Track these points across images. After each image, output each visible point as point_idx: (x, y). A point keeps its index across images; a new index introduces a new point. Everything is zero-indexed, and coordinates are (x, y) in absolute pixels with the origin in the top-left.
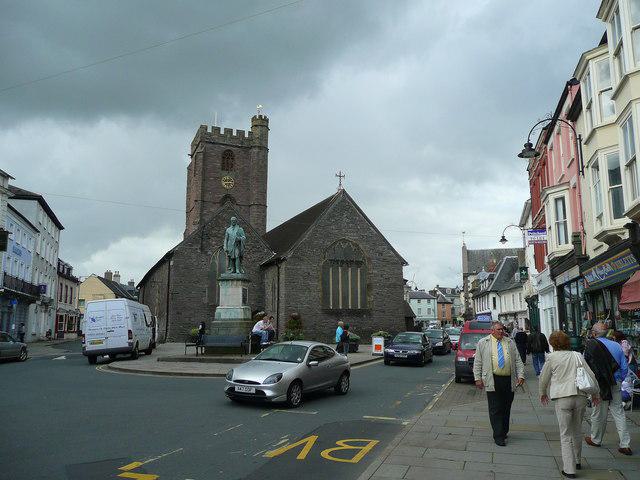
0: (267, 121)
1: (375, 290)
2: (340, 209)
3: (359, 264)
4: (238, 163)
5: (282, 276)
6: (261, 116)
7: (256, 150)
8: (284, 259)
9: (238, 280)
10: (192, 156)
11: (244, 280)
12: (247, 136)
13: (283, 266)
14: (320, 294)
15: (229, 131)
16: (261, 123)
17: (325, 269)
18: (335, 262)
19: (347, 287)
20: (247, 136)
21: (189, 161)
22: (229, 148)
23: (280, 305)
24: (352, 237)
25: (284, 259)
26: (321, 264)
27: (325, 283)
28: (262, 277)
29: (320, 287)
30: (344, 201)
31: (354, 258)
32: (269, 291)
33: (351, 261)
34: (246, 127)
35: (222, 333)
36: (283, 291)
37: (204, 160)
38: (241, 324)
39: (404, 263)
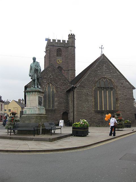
0: (75, 36)
1: (119, 102)
2: (102, 64)
3: (112, 89)
4: (63, 54)
5: (75, 95)
6: (72, 34)
7: (70, 48)
8: (76, 87)
9: (35, 91)
10: (46, 52)
11: (39, 92)
12: (66, 42)
13: (75, 90)
14: (93, 103)
15: (59, 41)
16: (72, 37)
17: (95, 91)
18: (100, 88)
19: (74, 37)
20: (66, 42)
21: (45, 54)
22: (59, 47)
23: (75, 108)
24: (108, 76)
25: (76, 87)
26: (94, 89)
27: (96, 98)
28: (68, 97)
29: (93, 100)
30: (103, 59)
31: (110, 86)
32: (70, 103)
33: (109, 88)
34: (66, 39)
35: (27, 122)
36: (75, 103)
37: (50, 53)
38: (37, 117)
39: (134, 88)
